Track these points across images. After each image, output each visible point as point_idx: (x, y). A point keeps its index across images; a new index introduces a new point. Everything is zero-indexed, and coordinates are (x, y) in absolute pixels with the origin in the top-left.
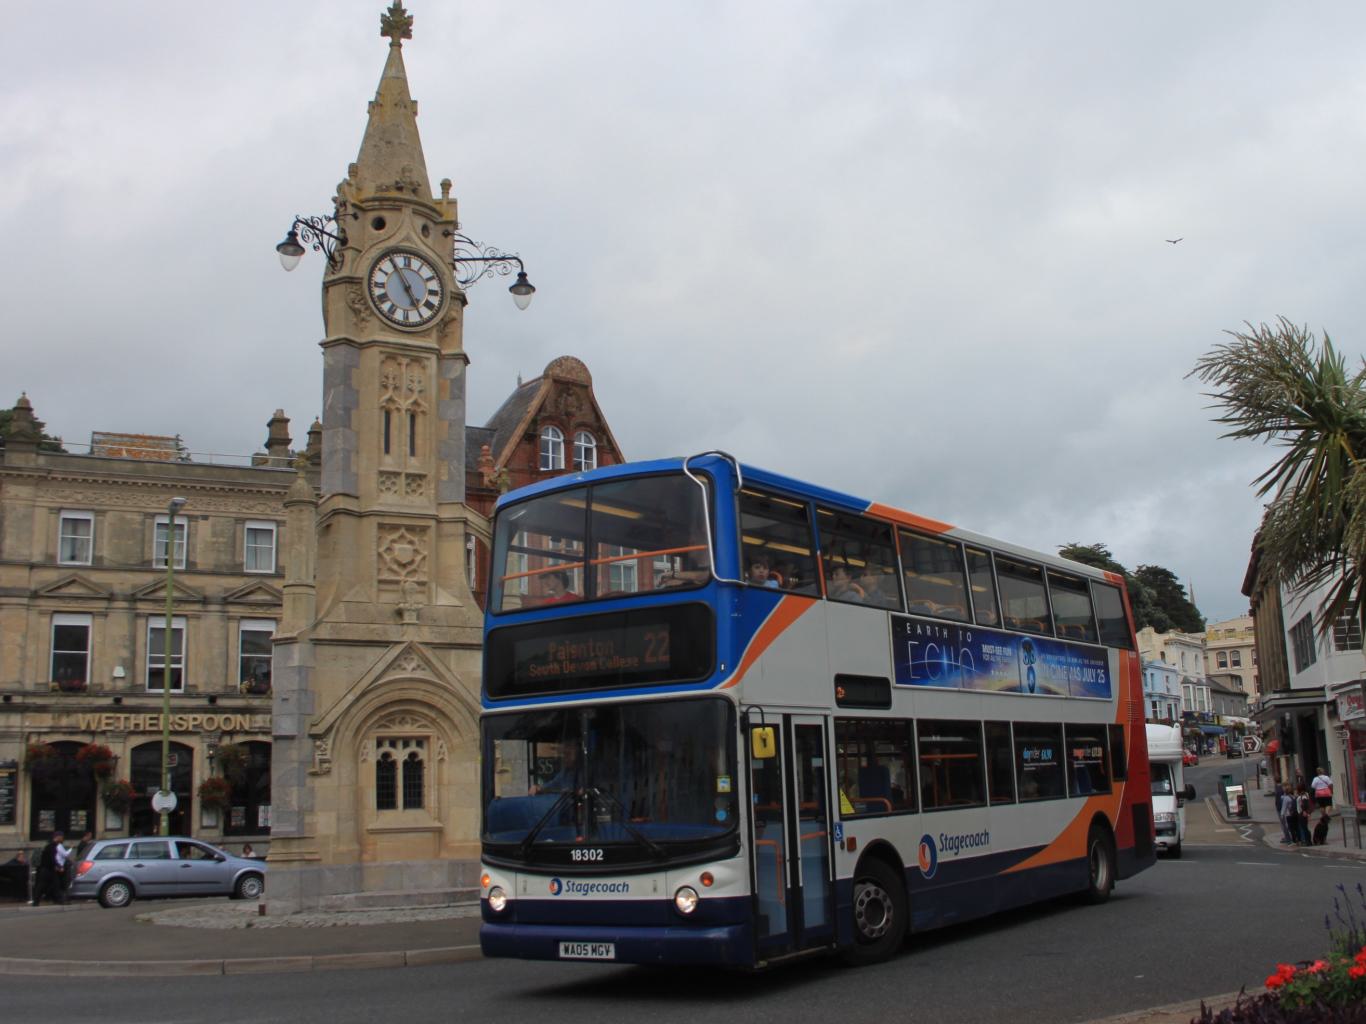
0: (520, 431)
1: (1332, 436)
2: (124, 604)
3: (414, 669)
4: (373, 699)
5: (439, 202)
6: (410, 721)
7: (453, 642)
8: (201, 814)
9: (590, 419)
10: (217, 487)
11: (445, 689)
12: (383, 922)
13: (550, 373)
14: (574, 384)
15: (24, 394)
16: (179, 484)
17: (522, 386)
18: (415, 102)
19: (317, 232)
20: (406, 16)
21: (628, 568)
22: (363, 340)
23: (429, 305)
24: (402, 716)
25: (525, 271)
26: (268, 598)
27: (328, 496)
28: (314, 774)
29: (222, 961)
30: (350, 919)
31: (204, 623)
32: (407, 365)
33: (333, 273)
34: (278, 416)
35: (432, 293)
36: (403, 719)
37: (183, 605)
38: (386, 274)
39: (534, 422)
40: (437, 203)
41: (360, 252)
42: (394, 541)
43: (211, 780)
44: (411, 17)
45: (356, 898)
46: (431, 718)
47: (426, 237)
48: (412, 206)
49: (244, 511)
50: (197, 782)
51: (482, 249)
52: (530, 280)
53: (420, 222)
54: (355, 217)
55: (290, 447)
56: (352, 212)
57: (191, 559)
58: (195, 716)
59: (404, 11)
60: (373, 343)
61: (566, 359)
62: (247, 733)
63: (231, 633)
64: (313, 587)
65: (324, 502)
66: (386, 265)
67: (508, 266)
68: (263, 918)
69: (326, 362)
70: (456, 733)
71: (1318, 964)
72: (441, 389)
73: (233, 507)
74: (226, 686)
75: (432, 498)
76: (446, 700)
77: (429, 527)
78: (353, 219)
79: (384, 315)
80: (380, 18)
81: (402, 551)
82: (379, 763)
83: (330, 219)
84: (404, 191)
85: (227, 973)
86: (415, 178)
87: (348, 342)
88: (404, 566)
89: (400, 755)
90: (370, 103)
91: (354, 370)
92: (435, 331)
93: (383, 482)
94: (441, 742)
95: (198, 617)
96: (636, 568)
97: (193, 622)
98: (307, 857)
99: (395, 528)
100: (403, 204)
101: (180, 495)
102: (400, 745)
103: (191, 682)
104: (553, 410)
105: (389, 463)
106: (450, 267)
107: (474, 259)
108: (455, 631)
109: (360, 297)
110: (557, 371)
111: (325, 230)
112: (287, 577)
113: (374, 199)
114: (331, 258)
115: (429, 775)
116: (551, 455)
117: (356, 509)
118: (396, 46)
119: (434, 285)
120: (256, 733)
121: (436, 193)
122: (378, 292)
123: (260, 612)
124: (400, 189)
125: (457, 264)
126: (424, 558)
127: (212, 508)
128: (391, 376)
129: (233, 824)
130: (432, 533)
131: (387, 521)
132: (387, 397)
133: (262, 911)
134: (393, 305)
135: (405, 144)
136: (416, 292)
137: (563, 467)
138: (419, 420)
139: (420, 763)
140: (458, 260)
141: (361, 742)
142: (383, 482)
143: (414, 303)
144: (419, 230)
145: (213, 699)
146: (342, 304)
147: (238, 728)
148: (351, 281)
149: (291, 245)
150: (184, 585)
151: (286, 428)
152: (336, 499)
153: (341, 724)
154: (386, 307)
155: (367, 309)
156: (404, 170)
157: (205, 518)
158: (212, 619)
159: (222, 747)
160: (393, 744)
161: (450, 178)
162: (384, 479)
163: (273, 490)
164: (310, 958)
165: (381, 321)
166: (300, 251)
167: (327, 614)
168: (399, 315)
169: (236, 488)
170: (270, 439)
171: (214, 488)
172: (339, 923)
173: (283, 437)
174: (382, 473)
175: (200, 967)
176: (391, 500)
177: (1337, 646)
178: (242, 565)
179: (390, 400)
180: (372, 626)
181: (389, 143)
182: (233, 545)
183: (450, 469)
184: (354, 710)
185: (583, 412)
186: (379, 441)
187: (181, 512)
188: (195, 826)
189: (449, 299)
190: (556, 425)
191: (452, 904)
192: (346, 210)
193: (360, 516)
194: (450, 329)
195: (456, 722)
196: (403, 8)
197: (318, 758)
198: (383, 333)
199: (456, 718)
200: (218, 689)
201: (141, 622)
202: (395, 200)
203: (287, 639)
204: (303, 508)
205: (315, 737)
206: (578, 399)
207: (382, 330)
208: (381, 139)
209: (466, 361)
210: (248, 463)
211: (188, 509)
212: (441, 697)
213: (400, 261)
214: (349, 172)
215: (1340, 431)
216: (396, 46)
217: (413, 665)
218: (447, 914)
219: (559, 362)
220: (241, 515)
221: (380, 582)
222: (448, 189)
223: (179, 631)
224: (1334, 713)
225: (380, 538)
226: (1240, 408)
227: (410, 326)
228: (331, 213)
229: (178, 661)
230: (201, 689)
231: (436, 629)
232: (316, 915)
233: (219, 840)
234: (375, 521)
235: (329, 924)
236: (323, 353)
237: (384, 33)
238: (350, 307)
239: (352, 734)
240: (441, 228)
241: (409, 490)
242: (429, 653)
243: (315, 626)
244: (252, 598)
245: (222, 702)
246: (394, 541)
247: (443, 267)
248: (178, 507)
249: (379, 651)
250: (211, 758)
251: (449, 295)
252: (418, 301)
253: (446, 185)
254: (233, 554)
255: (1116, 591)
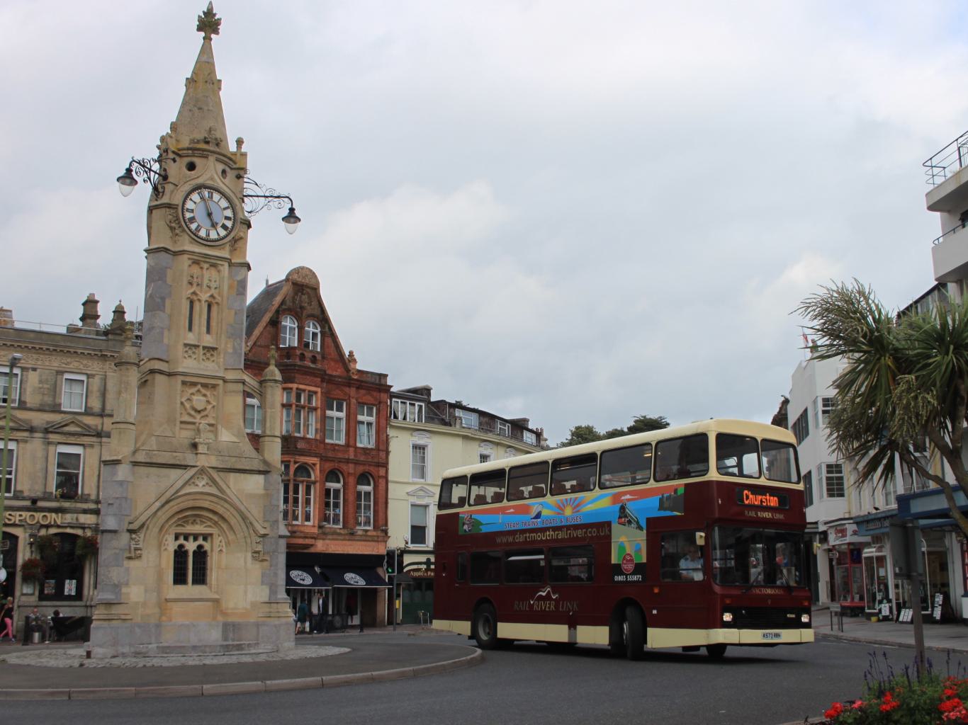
0: (267, 318)
1: (883, 358)
2: (40, 435)
3: (204, 486)
4: (173, 506)
5: (235, 154)
6: (199, 522)
7: (232, 467)
8: (22, 585)
9: (317, 312)
10: (45, 347)
11: (226, 501)
12: (178, 664)
13: (290, 278)
14: (307, 286)
15: (120, 301)
16: (16, 344)
17: (268, 286)
18: (220, 81)
19: (147, 170)
20: (216, 18)
21: (339, 419)
22: (177, 249)
23: (224, 227)
24: (193, 519)
25: (294, 207)
26: (78, 429)
27: (147, 359)
28: (130, 558)
29: (68, 690)
30: (156, 662)
31: (29, 446)
32: (207, 269)
33: (157, 200)
34: (91, 299)
35: (227, 218)
36: (195, 521)
37: (15, 433)
38: (195, 203)
39: (277, 312)
40: (232, 154)
41: (177, 186)
42: (193, 394)
43: (30, 560)
44: (220, 19)
45: (157, 647)
46: (214, 521)
47: (225, 178)
48: (216, 156)
49: (64, 366)
50: (20, 562)
51: (264, 189)
52: (297, 213)
53: (220, 167)
54: (174, 160)
55: (98, 321)
56: (172, 157)
57: (23, 399)
58: (21, 513)
59: (215, 15)
60: (183, 252)
61: (303, 268)
62: (59, 527)
63: (50, 455)
64: (134, 424)
65: (144, 364)
66: (195, 197)
67: (282, 202)
68: (89, 660)
69: (148, 264)
70: (232, 532)
71: (858, 703)
72: (230, 287)
73: (56, 362)
74: (45, 492)
75: (221, 364)
76: (225, 508)
77: (218, 385)
78: (172, 162)
79: (192, 233)
80: (197, 18)
81: (199, 401)
82: (175, 551)
83: (156, 161)
84: (211, 144)
85: (72, 698)
86: (218, 135)
87: (166, 250)
88: (199, 412)
89: (191, 546)
90: (187, 79)
91: (168, 270)
92: (228, 245)
93: (186, 352)
94: (220, 538)
95: (26, 442)
96: (344, 419)
97: (21, 445)
98: (123, 617)
99: (194, 384)
100: (209, 153)
101: (16, 352)
102: (191, 539)
103: (19, 488)
104: (291, 304)
105: (191, 338)
106: (241, 200)
107: (258, 196)
108: (234, 459)
109: (175, 218)
110: (295, 276)
111: (152, 169)
112: (115, 416)
113: (188, 149)
114: (155, 188)
115: (213, 561)
116: (288, 336)
117: (167, 371)
118: (207, 39)
119: (229, 213)
120: (66, 527)
121: (233, 147)
122: (188, 215)
123: (72, 439)
124: (207, 143)
125: (245, 199)
126: (214, 407)
127: (39, 363)
128: (195, 276)
129: (46, 592)
130: (221, 388)
131: (188, 379)
132: (192, 291)
133: (89, 655)
134: (199, 226)
135: (211, 111)
136: (216, 217)
137: (296, 345)
138: (214, 309)
139: (205, 552)
140: (246, 196)
141: (164, 536)
142: (186, 352)
143: (214, 225)
144: (220, 174)
145: (34, 501)
146: (163, 223)
147: (52, 523)
148: (169, 206)
149: (128, 178)
150: (16, 418)
151: (96, 307)
152: (152, 362)
153: (150, 523)
154: (193, 226)
155: (180, 227)
156: (210, 130)
157: (34, 370)
158: (36, 445)
159: (40, 537)
160: (186, 538)
161: (242, 137)
162: (187, 349)
163: (86, 352)
164: (133, 688)
165: (191, 237)
166: (134, 182)
167: (143, 444)
168: (203, 233)
169: (59, 349)
170: (83, 315)
171: (42, 349)
172: (149, 665)
173: (94, 314)
174: (186, 345)
175: (52, 694)
176: (189, 365)
177: (828, 494)
178: (60, 405)
179: (194, 293)
180: (175, 454)
181: (200, 109)
182: (55, 390)
183: (234, 344)
184: (159, 513)
185: (312, 307)
186: (185, 322)
187: (19, 365)
188: (17, 593)
189: (239, 223)
190: (292, 315)
191: (226, 653)
192: (167, 155)
193: (170, 375)
194: (240, 244)
195: (232, 524)
196: (214, 12)
197: (133, 547)
198: (191, 245)
199: (233, 521)
200: (39, 494)
201: (51, 448)
202: (204, 150)
203: (113, 461)
204: (129, 367)
205: (131, 531)
206: (309, 297)
207: (191, 243)
208: (195, 106)
209: (249, 268)
210: (64, 331)
211: (22, 364)
212: (222, 506)
213: (206, 193)
214: (171, 128)
215: (887, 355)
216: (207, 39)
217: (204, 482)
218: (224, 660)
219: (297, 271)
220: (60, 369)
221: (182, 422)
222: (241, 145)
223: (12, 451)
224: (824, 537)
225: (183, 391)
226: (824, 336)
227: (210, 241)
228: (156, 154)
229: (10, 473)
230: (26, 494)
231: (220, 458)
232: (129, 659)
233: (35, 604)
234: (180, 378)
235: (141, 665)
236: (146, 257)
237: (200, 29)
238: (168, 225)
239: (157, 530)
240: (235, 173)
241: (187, 356)
242: (215, 475)
243: (134, 452)
244: (66, 429)
245: (40, 504)
246: (193, 394)
247: (235, 201)
248: (17, 362)
249: (179, 472)
250: (31, 544)
251: (239, 221)
252: (217, 224)
253: (240, 142)
254: (54, 397)
255: (199, 409)
